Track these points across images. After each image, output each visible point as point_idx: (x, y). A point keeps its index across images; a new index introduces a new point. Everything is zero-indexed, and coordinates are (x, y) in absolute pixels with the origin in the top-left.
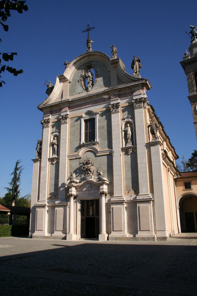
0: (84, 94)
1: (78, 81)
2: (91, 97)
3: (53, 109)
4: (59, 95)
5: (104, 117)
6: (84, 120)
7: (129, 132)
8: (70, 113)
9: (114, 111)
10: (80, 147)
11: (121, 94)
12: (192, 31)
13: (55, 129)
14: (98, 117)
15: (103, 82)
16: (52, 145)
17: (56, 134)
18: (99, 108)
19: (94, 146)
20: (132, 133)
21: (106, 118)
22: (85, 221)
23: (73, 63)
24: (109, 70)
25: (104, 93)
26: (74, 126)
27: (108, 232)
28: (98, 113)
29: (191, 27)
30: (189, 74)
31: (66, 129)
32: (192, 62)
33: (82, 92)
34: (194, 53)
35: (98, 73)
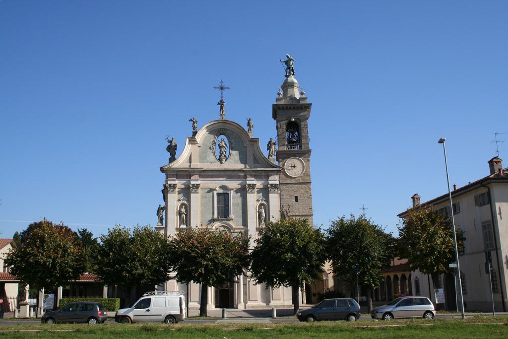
0: (216, 166)
1: (210, 148)
2: (226, 171)
3: (178, 173)
4: (187, 158)
5: (239, 194)
6: (217, 193)
7: (264, 214)
8: (204, 183)
9: (250, 190)
10: (213, 220)
11: (257, 176)
12: (288, 61)
13: (181, 196)
14: (232, 193)
15: (238, 157)
16: (180, 213)
17: (183, 202)
18: (234, 184)
19: (228, 222)
20: (265, 215)
21: (241, 196)
22: (219, 293)
23: (206, 126)
24: (245, 146)
25: (241, 171)
26: (206, 198)
27: (245, 302)
28: (233, 190)
29: (288, 57)
30: (281, 122)
31: (196, 199)
32: (287, 108)
33: (214, 162)
34: (288, 95)
35: (233, 145)
